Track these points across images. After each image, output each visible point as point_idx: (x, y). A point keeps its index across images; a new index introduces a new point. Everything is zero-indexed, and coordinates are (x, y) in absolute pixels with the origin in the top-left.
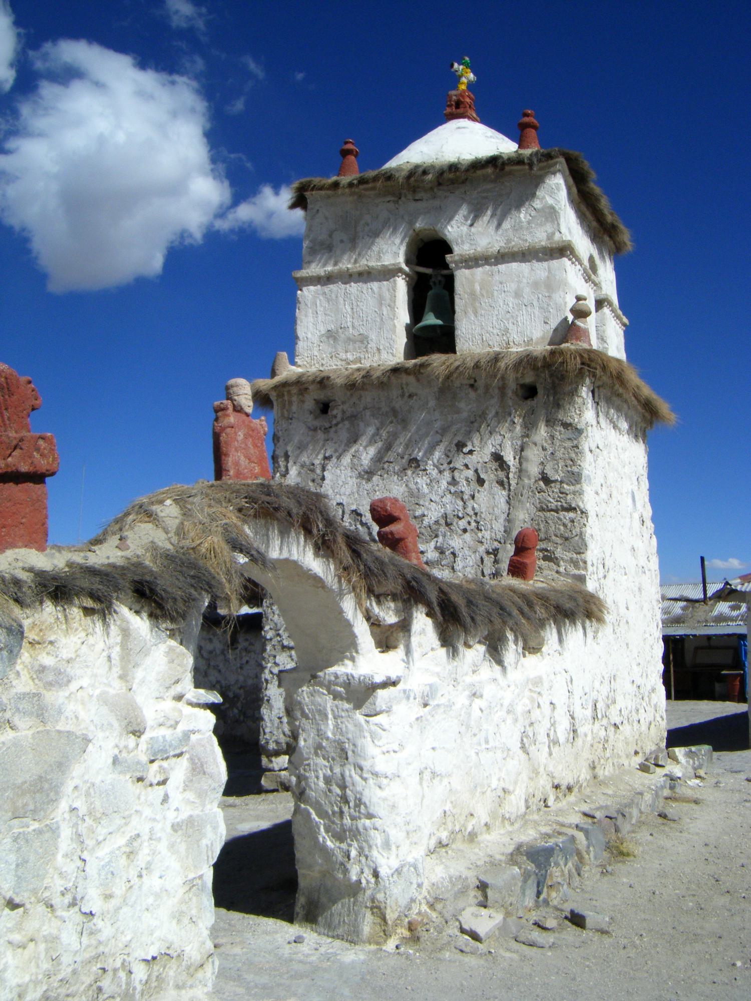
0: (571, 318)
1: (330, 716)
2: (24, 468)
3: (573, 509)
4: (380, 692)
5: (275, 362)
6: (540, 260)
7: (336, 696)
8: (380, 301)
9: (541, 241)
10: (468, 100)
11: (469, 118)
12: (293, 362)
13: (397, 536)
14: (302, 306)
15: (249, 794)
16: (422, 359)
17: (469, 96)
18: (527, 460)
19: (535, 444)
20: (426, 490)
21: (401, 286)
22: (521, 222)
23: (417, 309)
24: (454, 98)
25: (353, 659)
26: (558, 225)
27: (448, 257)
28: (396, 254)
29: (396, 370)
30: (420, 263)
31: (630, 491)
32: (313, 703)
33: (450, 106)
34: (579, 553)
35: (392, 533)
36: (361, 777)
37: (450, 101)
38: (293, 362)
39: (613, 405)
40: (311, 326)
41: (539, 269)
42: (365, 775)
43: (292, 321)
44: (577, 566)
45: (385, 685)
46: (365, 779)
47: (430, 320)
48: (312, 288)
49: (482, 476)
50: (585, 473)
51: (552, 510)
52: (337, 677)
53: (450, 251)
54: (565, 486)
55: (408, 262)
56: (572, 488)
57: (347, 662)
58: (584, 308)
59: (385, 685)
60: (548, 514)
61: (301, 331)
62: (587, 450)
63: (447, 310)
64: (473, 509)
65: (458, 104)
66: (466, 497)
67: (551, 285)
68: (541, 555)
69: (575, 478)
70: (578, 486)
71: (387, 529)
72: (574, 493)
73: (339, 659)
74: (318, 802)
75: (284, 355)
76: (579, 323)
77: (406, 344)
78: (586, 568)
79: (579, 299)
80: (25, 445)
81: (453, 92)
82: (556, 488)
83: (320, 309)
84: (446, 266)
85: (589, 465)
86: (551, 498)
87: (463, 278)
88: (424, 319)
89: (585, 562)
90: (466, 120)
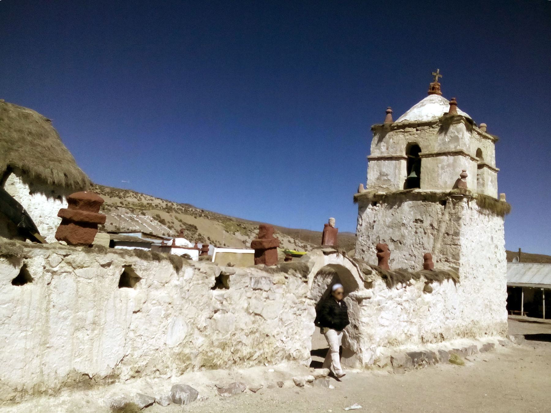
0: (460, 178)
1: (351, 305)
2: (272, 246)
3: (457, 245)
4: (364, 300)
5: (359, 187)
6: (451, 155)
7: (353, 300)
8: (396, 167)
9: (452, 149)
10: (437, 87)
11: (437, 94)
12: (366, 188)
13: (381, 256)
14: (369, 168)
15: (531, 335)
16: (408, 190)
17: (438, 85)
18: (441, 227)
19: (444, 222)
20: (407, 234)
21: (404, 163)
22: (446, 141)
23: (409, 172)
24: (432, 86)
25: (358, 290)
26: (459, 143)
27: (419, 154)
28: (401, 151)
29: (401, 193)
30: (411, 154)
31: (490, 236)
32: (347, 302)
33: (430, 89)
34: (458, 260)
35: (380, 255)
36: (358, 323)
37: (431, 87)
38: (366, 188)
39: (99, 385)
40: (372, 175)
41: (451, 158)
42: (359, 322)
43: (366, 173)
44: (456, 265)
45: (366, 298)
46: (359, 323)
47: (413, 175)
48: (373, 162)
49: (425, 231)
50: (461, 232)
51: (449, 245)
52: (353, 295)
53: (420, 151)
54: (454, 237)
55: (406, 154)
56: (456, 238)
57: (356, 291)
58: (466, 175)
59: (366, 298)
60: (448, 246)
61: (369, 176)
62: (462, 224)
63: (418, 172)
64: (422, 242)
65: (433, 88)
66: (420, 238)
67: (453, 166)
68: (444, 260)
69: (457, 234)
70: (458, 237)
71: (380, 254)
72: (457, 239)
73: (353, 290)
74: (347, 329)
75: (362, 185)
76: (463, 180)
77: (405, 183)
78: (459, 266)
79: (463, 171)
80: (272, 241)
81: (432, 84)
82: (451, 236)
83: (375, 170)
84: (419, 156)
85: (463, 229)
86: (448, 240)
87: (425, 163)
88: (411, 174)
89: (459, 264)
90: (436, 95)
